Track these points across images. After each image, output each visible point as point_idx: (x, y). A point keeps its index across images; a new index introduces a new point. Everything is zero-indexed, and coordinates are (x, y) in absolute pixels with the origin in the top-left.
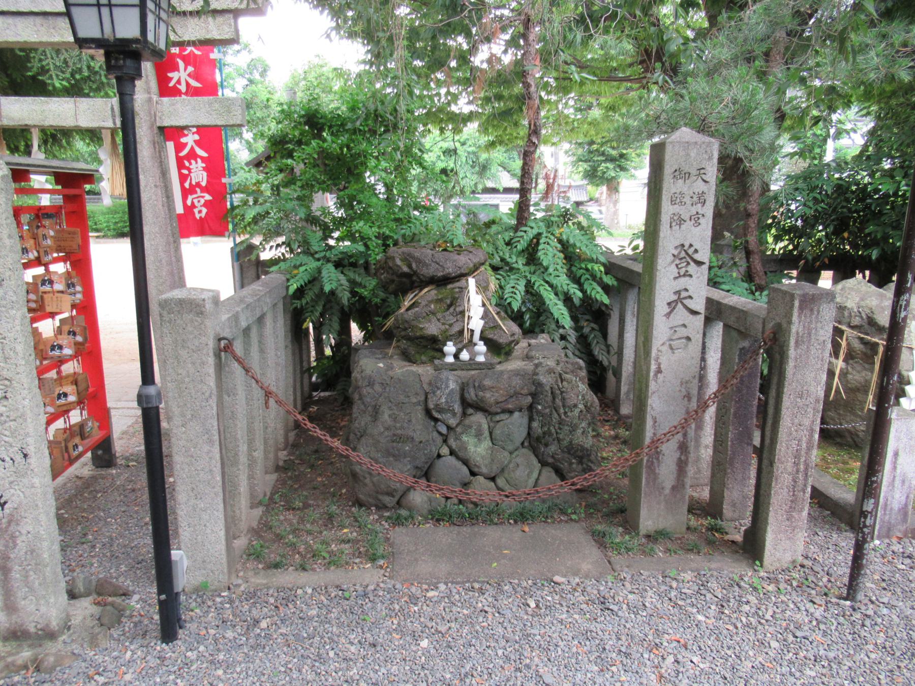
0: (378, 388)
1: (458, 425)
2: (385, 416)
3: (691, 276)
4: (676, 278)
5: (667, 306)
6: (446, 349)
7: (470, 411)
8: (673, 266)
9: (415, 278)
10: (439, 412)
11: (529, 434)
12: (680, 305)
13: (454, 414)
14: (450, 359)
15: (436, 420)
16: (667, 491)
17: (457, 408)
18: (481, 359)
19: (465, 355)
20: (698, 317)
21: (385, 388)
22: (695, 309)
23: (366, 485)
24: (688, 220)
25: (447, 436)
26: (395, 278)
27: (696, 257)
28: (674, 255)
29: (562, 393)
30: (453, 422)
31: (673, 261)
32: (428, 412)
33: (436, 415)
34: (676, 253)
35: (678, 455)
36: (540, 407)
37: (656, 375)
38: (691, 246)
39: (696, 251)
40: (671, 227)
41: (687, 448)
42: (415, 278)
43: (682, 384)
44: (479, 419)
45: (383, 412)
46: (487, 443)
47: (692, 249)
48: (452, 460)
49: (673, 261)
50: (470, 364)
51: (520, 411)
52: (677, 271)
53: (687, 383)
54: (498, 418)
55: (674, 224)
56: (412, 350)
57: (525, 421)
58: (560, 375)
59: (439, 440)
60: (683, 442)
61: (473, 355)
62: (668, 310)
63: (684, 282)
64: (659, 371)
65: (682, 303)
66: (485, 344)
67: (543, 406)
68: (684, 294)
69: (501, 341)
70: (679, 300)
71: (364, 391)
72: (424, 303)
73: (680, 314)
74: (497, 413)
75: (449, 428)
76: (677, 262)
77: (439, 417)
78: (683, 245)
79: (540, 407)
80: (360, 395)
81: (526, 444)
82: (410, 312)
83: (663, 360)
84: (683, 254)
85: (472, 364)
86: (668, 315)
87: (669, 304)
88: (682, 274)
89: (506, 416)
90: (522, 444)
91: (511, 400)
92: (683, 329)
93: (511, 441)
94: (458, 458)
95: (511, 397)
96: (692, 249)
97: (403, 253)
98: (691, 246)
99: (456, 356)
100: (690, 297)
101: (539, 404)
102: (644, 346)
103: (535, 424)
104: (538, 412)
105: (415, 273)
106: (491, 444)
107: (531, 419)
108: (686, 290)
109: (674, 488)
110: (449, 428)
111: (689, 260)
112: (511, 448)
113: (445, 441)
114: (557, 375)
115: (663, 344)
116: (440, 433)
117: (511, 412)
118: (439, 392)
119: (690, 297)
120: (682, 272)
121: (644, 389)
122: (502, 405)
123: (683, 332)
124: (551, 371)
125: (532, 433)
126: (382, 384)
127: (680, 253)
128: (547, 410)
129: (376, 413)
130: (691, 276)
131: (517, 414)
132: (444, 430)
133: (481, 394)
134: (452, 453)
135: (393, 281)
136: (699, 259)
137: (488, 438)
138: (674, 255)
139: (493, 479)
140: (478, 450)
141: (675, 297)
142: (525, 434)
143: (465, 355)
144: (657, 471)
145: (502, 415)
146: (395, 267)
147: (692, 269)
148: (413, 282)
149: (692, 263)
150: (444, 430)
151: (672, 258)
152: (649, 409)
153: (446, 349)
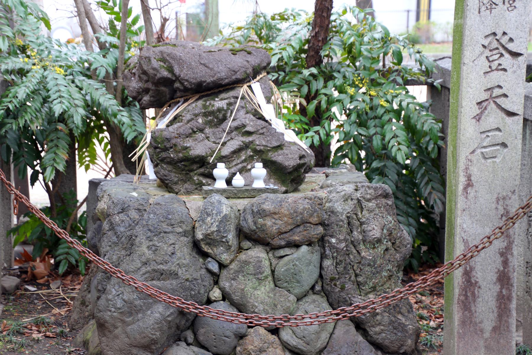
0: (134, 214)
1: (232, 261)
2: (143, 249)
3: (505, 70)
4: (486, 73)
5: (477, 107)
6: (216, 172)
7: (246, 244)
8: (483, 58)
9: (177, 85)
10: (209, 244)
11: (321, 276)
12: (493, 105)
13: (229, 248)
14: (221, 184)
15: (205, 255)
16: (487, 335)
17: (231, 237)
18: (259, 184)
19: (239, 181)
20: (516, 118)
21: (142, 216)
22: (511, 110)
23: (116, 337)
24: (501, 4)
25: (218, 276)
26: (150, 85)
27: (511, 47)
28: (484, 46)
29: (362, 224)
30: (225, 257)
31: (482, 54)
32: (196, 245)
33: (205, 248)
34: (486, 42)
35: (497, 288)
36: (333, 240)
37: (465, 189)
38: (504, 33)
39: (511, 40)
40: (479, 12)
41: (509, 279)
42: (177, 85)
43: (498, 200)
44: (257, 253)
45: (141, 243)
46: (269, 284)
47: (506, 38)
48: (223, 306)
49: (482, 54)
50: (247, 190)
51: (310, 244)
52: (488, 64)
53: (504, 198)
54: (282, 252)
55: (483, 9)
56: (174, 177)
57: (316, 257)
58: (359, 201)
59: (209, 280)
60: (503, 272)
61: (250, 181)
62: (478, 112)
63: (496, 77)
64: (469, 184)
65: (495, 103)
66: (265, 166)
67: (338, 239)
68: (497, 92)
69: (287, 164)
70: (493, 97)
71: (117, 219)
72: (188, 117)
73: (493, 118)
74: (281, 247)
75: (222, 266)
76: (487, 53)
77: (210, 251)
78: (494, 34)
79: (333, 240)
80: (112, 224)
81: (318, 288)
82: (170, 128)
83: (474, 171)
84: (495, 44)
85: (249, 192)
86: (478, 118)
87: (479, 103)
88: (494, 68)
89: (293, 250)
90: (313, 288)
91: (298, 230)
92: (497, 133)
93: (298, 282)
94: (233, 304)
95: (298, 226)
96: (506, 38)
97: (161, 52)
98: (504, 33)
99: (229, 182)
100: (505, 96)
101: (332, 236)
102: (453, 156)
103: (327, 263)
104: (332, 247)
105: (178, 78)
106: (272, 285)
107: (323, 256)
108: (500, 87)
109: (495, 329)
110: (222, 266)
111: (504, 52)
112: (297, 291)
113: (216, 283)
114: (356, 202)
115: (473, 152)
116: (209, 271)
117: (297, 246)
118: (209, 219)
119: (505, 96)
120: (494, 65)
121: (453, 207)
122: (287, 235)
123: (499, 137)
124: (347, 198)
125: (323, 273)
126: (139, 209)
127: (490, 43)
128: (343, 245)
129: (130, 245)
130: (505, 70)
131: (304, 249)
132: (215, 267)
133: (261, 220)
134: (225, 297)
135: (146, 91)
136: (514, 50)
137: (270, 278)
138: (484, 46)
139: (275, 331)
140: (260, 295)
141: (485, 96)
142: (316, 275)
143: (239, 181)
144: (473, 309)
145: (286, 249)
146: (151, 71)
147: (507, 61)
148: (174, 91)
149: (507, 55)
150: (215, 267)
151: (482, 49)
152: (458, 230)
153: (216, 172)
